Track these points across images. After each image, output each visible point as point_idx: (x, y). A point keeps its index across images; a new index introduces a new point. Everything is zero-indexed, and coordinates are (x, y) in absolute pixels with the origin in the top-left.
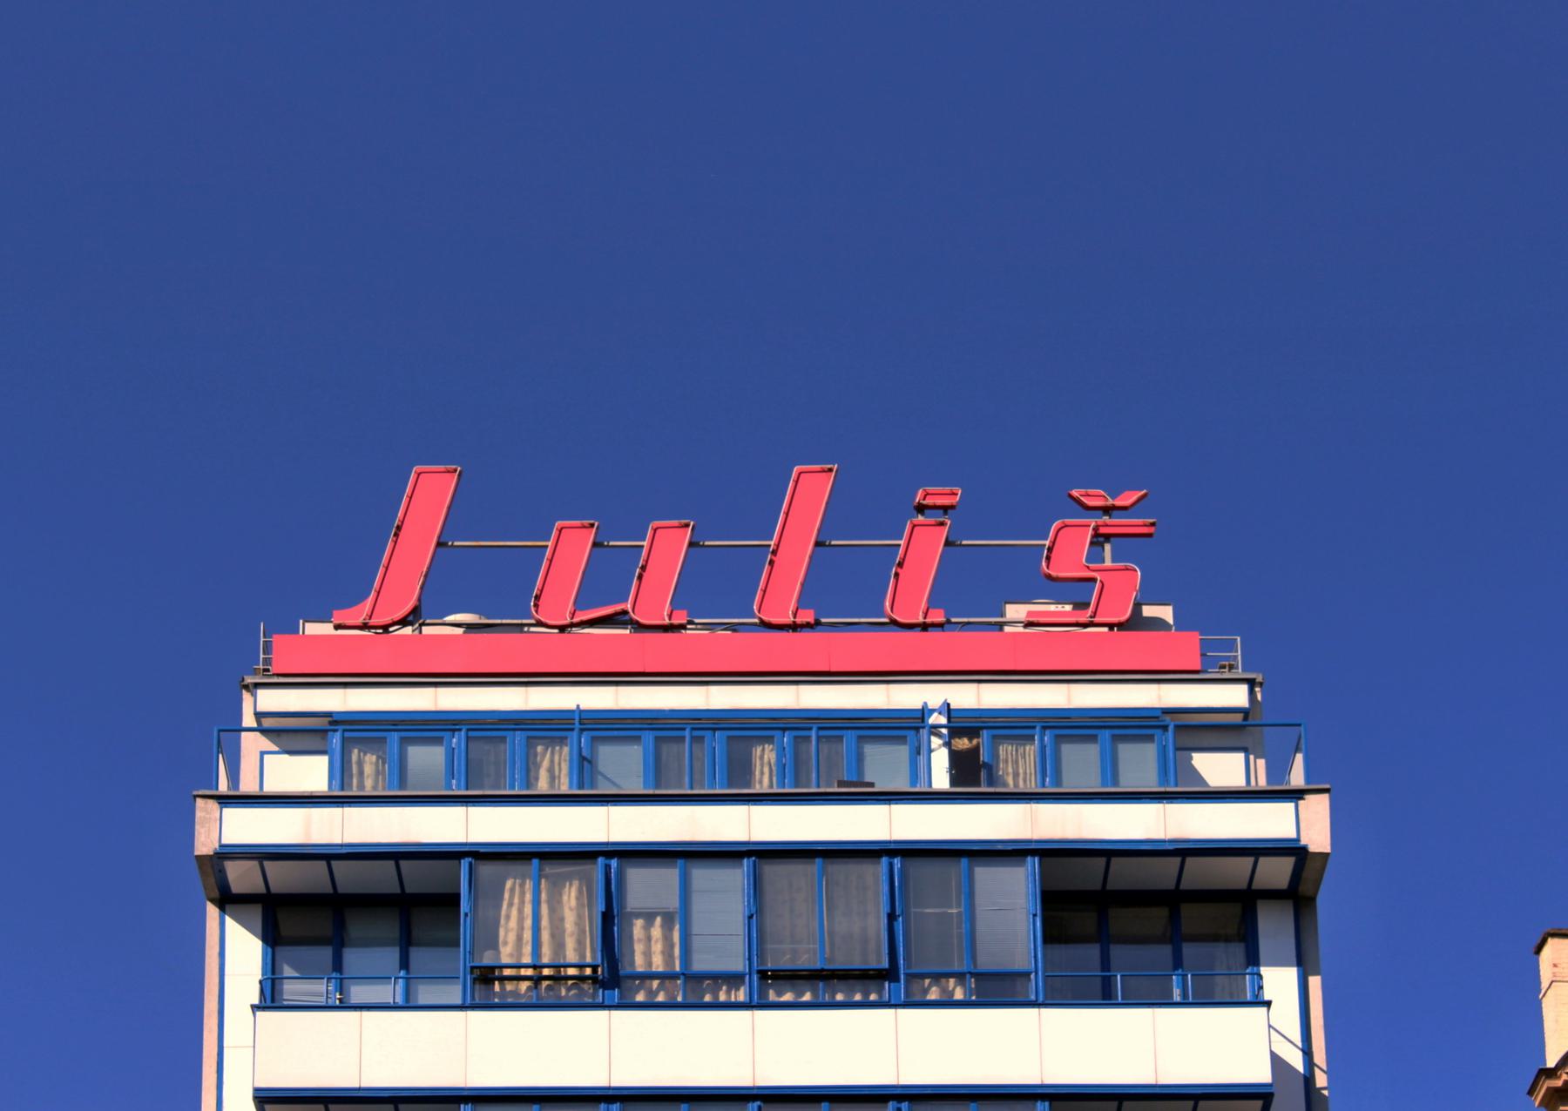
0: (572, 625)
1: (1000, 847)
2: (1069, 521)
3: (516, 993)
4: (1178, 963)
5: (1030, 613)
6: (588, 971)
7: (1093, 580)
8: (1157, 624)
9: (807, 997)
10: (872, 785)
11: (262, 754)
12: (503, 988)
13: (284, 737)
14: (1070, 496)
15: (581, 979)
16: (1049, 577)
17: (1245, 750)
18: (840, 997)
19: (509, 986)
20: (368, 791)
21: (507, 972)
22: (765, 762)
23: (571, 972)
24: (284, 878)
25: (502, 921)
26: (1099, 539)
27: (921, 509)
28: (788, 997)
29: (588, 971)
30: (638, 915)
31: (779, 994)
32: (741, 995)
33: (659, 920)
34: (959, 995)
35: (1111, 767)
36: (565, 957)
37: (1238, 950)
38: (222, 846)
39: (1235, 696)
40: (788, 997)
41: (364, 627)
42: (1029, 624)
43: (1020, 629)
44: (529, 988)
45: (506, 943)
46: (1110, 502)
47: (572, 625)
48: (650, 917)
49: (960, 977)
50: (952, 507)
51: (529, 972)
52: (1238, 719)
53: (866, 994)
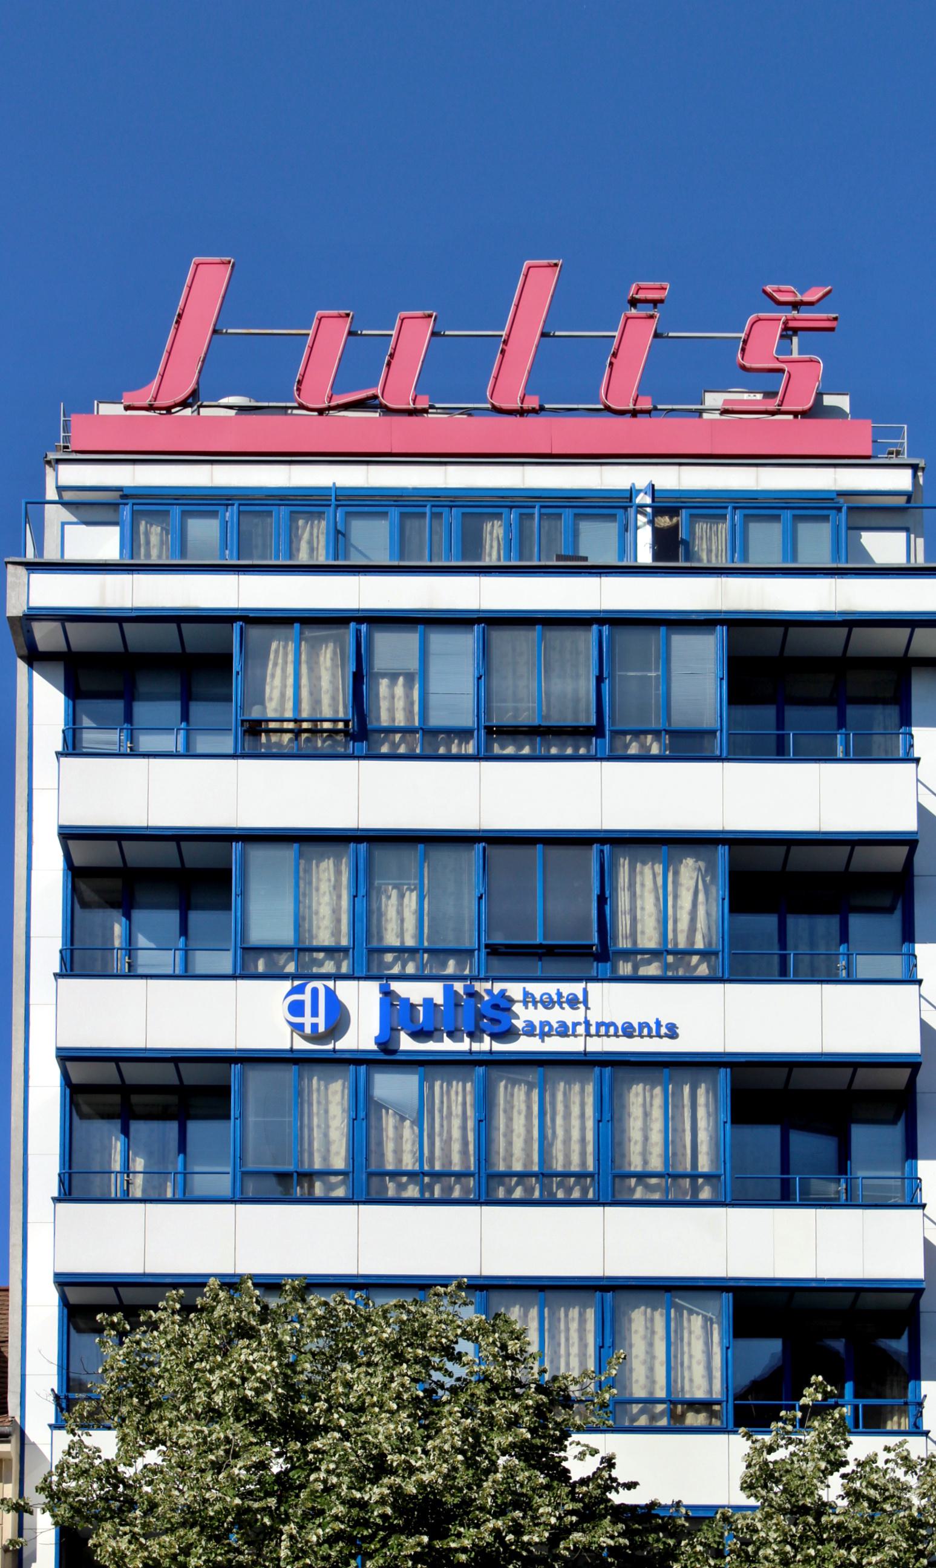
0: (330, 408)
1: (694, 617)
2: (762, 315)
3: (279, 744)
4: (842, 723)
5: (726, 402)
6: (341, 725)
7: (782, 371)
8: (835, 412)
9: (526, 751)
10: (585, 559)
11: (63, 524)
12: (269, 740)
13: (83, 509)
14: (765, 292)
15: (333, 732)
16: (744, 368)
17: (907, 529)
18: (554, 751)
19: (274, 738)
20: (154, 560)
21: (272, 725)
22: (494, 533)
23: (327, 725)
24: (83, 637)
25: (268, 679)
26: (789, 331)
27: (634, 302)
28: (510, 750)
29: (341, 725)
30: (384, 675)
31: (503, 747)
32: (470, 748)
33: (401, 680)
34: (655, 750)
35: (791, 546)
36: (321, 712)
37: (893, 712)
38: (29, 608)
39: (900, 480)
40: (510, 750)
41: (150, 408)
42: (724, 412)
43: (716, 416)
44: (290, 740)
45: (271, 699)
46: (799, 297)
47: (330, 408)
48: (393, 677)
49: (657, 733)
50: (661, 301)
51: (291, 725)
52: (901, 501)
53: (521, 748)
